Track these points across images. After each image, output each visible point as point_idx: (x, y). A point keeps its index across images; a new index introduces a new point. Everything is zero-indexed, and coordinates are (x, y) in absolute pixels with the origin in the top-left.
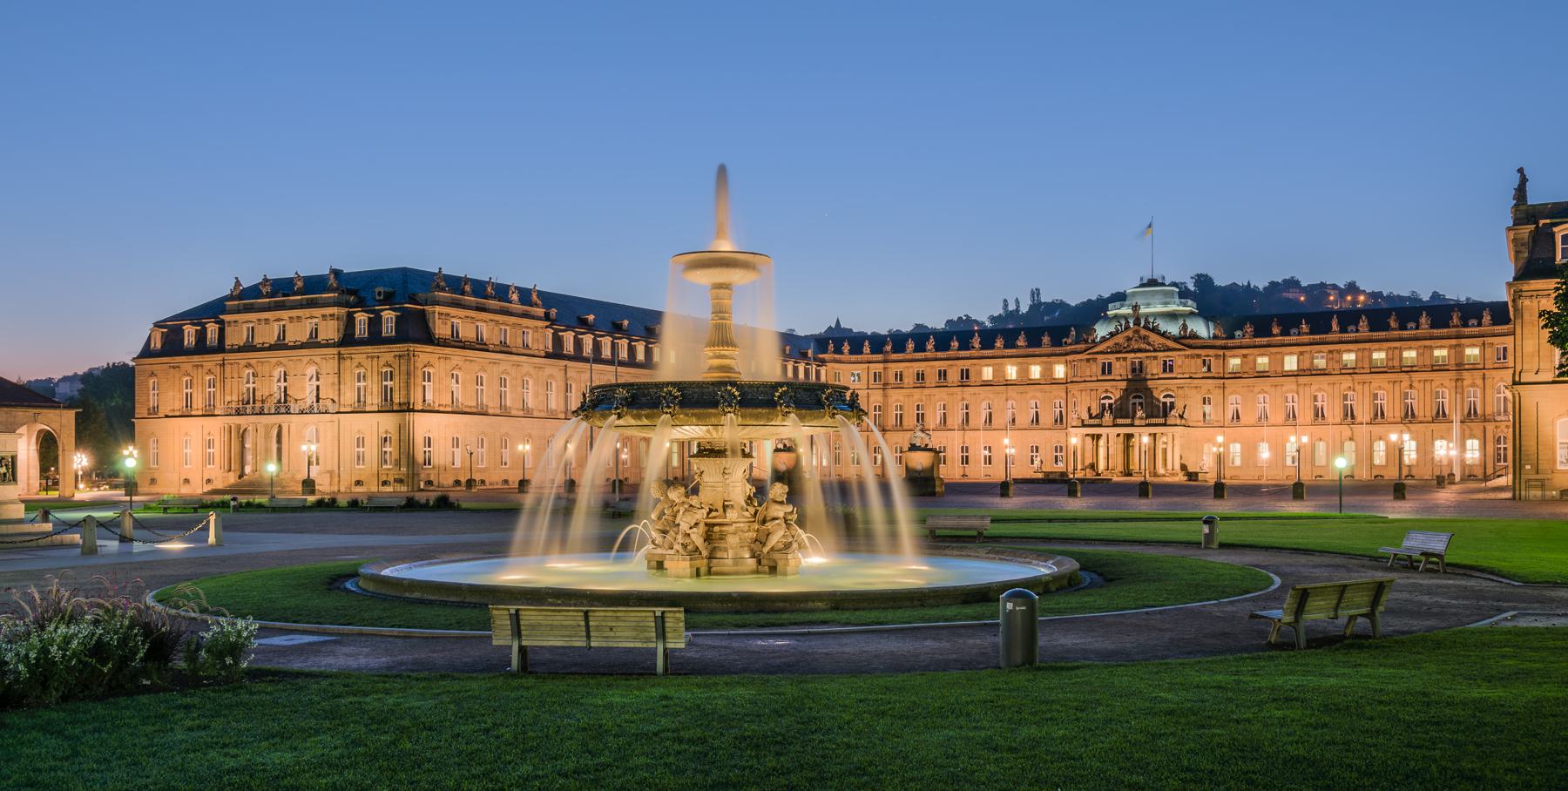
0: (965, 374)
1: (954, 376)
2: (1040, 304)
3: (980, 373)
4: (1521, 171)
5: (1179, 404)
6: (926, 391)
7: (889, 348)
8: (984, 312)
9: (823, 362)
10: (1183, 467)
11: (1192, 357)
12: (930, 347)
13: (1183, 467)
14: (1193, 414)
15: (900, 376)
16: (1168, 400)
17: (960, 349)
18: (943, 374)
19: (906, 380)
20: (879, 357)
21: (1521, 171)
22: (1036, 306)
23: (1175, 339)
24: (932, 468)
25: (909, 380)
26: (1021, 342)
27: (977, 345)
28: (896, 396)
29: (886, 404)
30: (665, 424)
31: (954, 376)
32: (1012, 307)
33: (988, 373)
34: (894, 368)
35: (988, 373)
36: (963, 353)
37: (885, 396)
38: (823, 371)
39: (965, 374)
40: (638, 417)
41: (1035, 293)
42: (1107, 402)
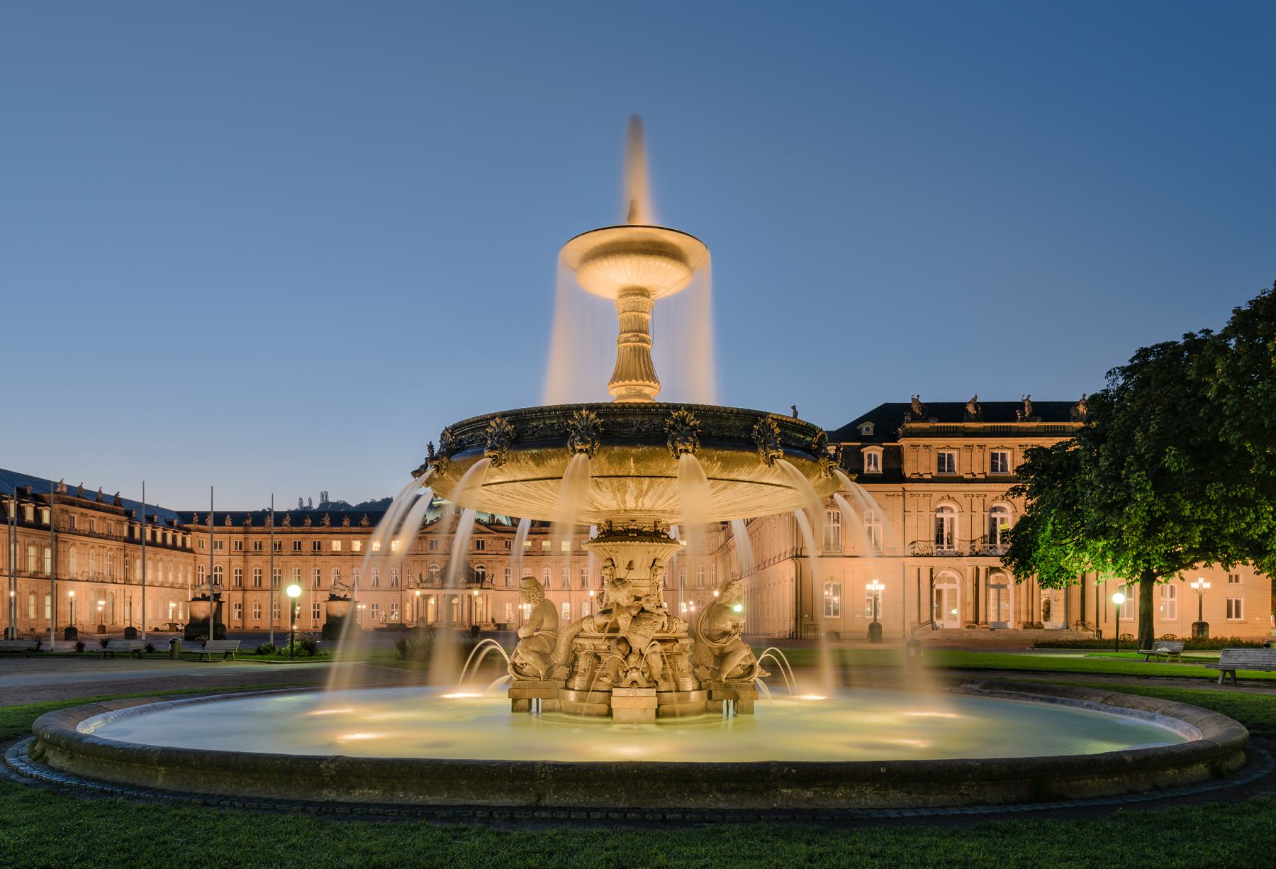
0: (317, 546)
1: (307, 546)
2: (328, 503)
3: (330, 545)
4: (794, 408)
5: (489, 572)
6: (283, 559)
7: (249, 522)
8: (286, 503)
9: (188, 531)
10: (493, 620)
11: (498, 538)
12: (286, 522)
13: (493, 620)
14: (499, 581)
15: (259, 546)
16: (480, 571)
17: (312, 525)
18: (298, 546)
19: (265, 549)
20: (240, 529)
21: (794, 408)
22: (325, 504)
23: (486, 525)
24: (1148, 579)
25: (267, 549)
26: (364, 522)
27: (327, 523)
28: (256, 563)
29: (246, 568)
30: (693, 473)
31: (307, 546)
32: (306, 504)
33: (337, 545)
34: (253, 538)
35: (337, 545)
36: (316, 529)
37: (246, 562)
38: (188, 538)
39: (317, 546)
40: (539, 461)
41: (324, 495)
42: (434, 570)
